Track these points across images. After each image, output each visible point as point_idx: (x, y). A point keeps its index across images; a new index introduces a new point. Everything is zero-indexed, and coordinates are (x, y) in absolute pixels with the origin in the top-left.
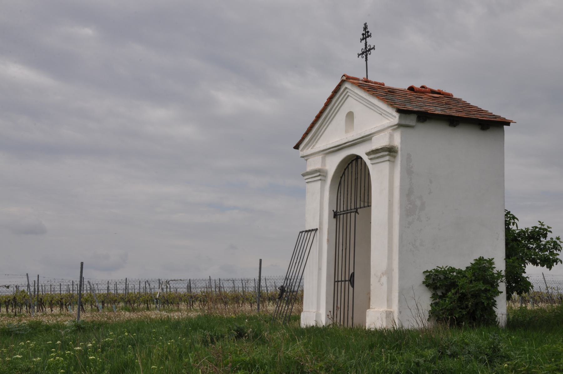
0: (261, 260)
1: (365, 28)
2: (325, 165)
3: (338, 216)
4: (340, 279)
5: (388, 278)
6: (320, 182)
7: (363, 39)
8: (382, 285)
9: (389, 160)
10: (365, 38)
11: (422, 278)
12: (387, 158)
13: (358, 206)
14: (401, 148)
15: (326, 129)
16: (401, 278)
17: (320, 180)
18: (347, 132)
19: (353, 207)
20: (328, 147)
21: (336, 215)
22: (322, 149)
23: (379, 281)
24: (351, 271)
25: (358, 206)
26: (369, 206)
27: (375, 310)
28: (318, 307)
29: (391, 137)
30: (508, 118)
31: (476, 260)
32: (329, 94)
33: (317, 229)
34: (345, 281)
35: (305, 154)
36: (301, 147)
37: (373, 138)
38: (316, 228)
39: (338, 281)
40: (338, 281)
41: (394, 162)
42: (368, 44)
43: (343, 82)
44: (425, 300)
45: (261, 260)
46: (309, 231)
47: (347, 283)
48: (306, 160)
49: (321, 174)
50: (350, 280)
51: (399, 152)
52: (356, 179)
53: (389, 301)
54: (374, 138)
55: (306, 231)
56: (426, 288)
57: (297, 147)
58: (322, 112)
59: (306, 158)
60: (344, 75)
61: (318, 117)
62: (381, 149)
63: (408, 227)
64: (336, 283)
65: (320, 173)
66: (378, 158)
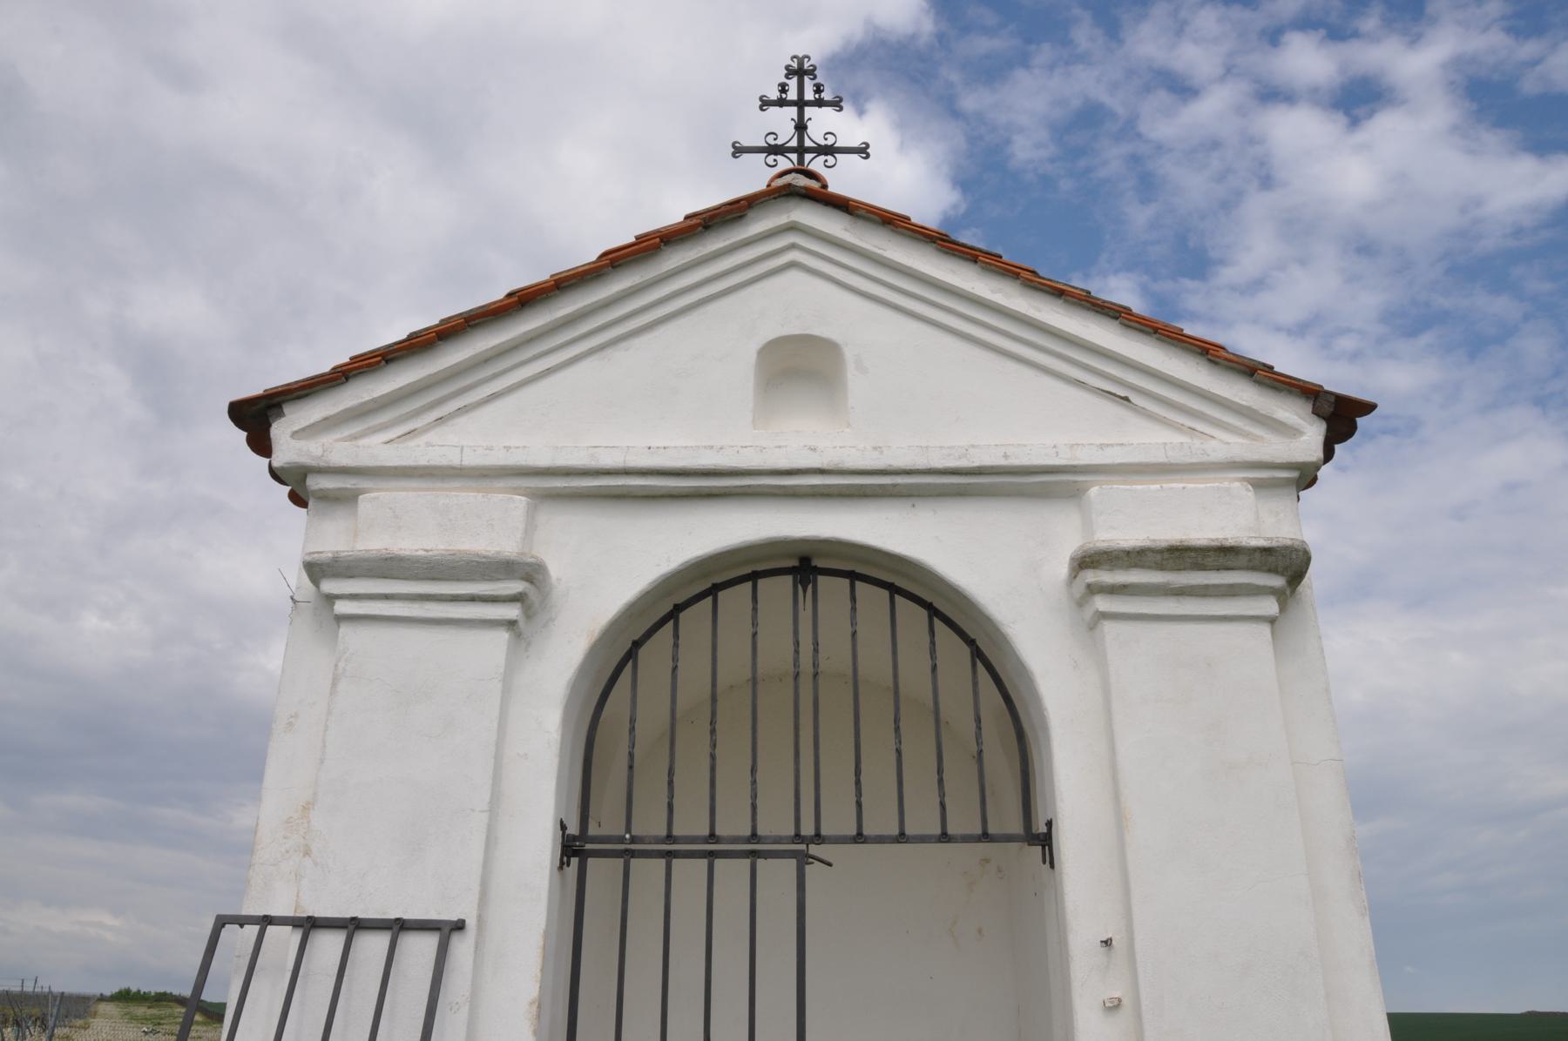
7: (781, 103)
10: (801, 104)
17: (511, 624)
21: (573, 849)
22: (543, 460)
33: (459, 926)
38: (453, 917)
49: (533, 595)
61: (523, 301)
65: (519, 589)
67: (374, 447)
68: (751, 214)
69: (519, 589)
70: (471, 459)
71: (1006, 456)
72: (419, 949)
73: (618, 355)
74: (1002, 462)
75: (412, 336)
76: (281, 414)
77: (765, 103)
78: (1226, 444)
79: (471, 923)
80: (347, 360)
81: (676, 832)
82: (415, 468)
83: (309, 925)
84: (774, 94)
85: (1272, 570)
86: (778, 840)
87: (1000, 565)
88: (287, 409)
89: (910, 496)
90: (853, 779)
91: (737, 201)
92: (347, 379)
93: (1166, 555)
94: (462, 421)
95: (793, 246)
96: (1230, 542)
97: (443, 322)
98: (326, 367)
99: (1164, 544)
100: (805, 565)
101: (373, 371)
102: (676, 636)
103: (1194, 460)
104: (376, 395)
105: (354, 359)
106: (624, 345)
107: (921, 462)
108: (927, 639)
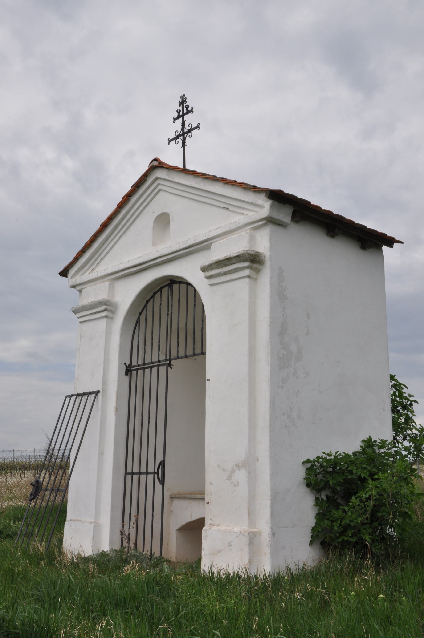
1: (183, 102)
3: (134, 373)
4: (136, 470)
5: (249, 473)
6: (105, 320)
7: (178, 118)
8: (236, 485)
9: (249, 277)
10: (183, 116)
11: (301, 473)
12: (247, 272)
13: (174, 354)
14: (270, 256)
15: (116, 243)
16: (274, 474)
17: (106, 317)
18: (154, 244)
19: (162, 357)
21: (129, 370)
22: (110, 271)
23: (229, 478)
24: (159, 459)
25: (174, 354)
27: (222, 528)
28: (97, 514)
29: (252, 239)
30: (389, 234)
31: (364, 441)
32: (128, 188)
33: (98, 392)
34: (147, 473)
35: (78, 282)
36: (72, 272)
37: (213, 245)
38: (96, 390)
39: (133, 474)
40: (133, 474)
41: (255, 279)
42: (187, 124)
43: (152, 169)
44: (305, 510)
46: (84, 394)
47: (151, 477)
48: (80, 291)
49: (108, 307)
50: (156, 473)
51: (268, 264)
52: (169, 315)
53: (251, 514)
55: (78, 395)
56: (307, 490)
57: (64, 273)
58: (111, 218)
59: (79, 288)
60: (156, 160)
61: (104, 226)
62: (238, 256)
63: (282, 387)
64: (129, 477)
65: (107, 307)
66: (225, 274)
67: (86, 276)
68: (148, 178)
69: (107, 307)
71: (195, 240)
72: (93, 396)
75: (86, 244)
76: (69, 273)
77: (175, 119)
78: (238, 219)
79: (101, 390)
80: (76, 255)
84: (176, 115)
85: (244, 261)
87: (189, 270)
89: (181, 257)
92: (78, 259)
95: (159, 184)
96: (229, 257)
97: (90, 238)
98: (72, 259)
99: (214, 262)
101: (82, 256)
102: (147, 311)
103: (236, 227)
106: (129, 229)
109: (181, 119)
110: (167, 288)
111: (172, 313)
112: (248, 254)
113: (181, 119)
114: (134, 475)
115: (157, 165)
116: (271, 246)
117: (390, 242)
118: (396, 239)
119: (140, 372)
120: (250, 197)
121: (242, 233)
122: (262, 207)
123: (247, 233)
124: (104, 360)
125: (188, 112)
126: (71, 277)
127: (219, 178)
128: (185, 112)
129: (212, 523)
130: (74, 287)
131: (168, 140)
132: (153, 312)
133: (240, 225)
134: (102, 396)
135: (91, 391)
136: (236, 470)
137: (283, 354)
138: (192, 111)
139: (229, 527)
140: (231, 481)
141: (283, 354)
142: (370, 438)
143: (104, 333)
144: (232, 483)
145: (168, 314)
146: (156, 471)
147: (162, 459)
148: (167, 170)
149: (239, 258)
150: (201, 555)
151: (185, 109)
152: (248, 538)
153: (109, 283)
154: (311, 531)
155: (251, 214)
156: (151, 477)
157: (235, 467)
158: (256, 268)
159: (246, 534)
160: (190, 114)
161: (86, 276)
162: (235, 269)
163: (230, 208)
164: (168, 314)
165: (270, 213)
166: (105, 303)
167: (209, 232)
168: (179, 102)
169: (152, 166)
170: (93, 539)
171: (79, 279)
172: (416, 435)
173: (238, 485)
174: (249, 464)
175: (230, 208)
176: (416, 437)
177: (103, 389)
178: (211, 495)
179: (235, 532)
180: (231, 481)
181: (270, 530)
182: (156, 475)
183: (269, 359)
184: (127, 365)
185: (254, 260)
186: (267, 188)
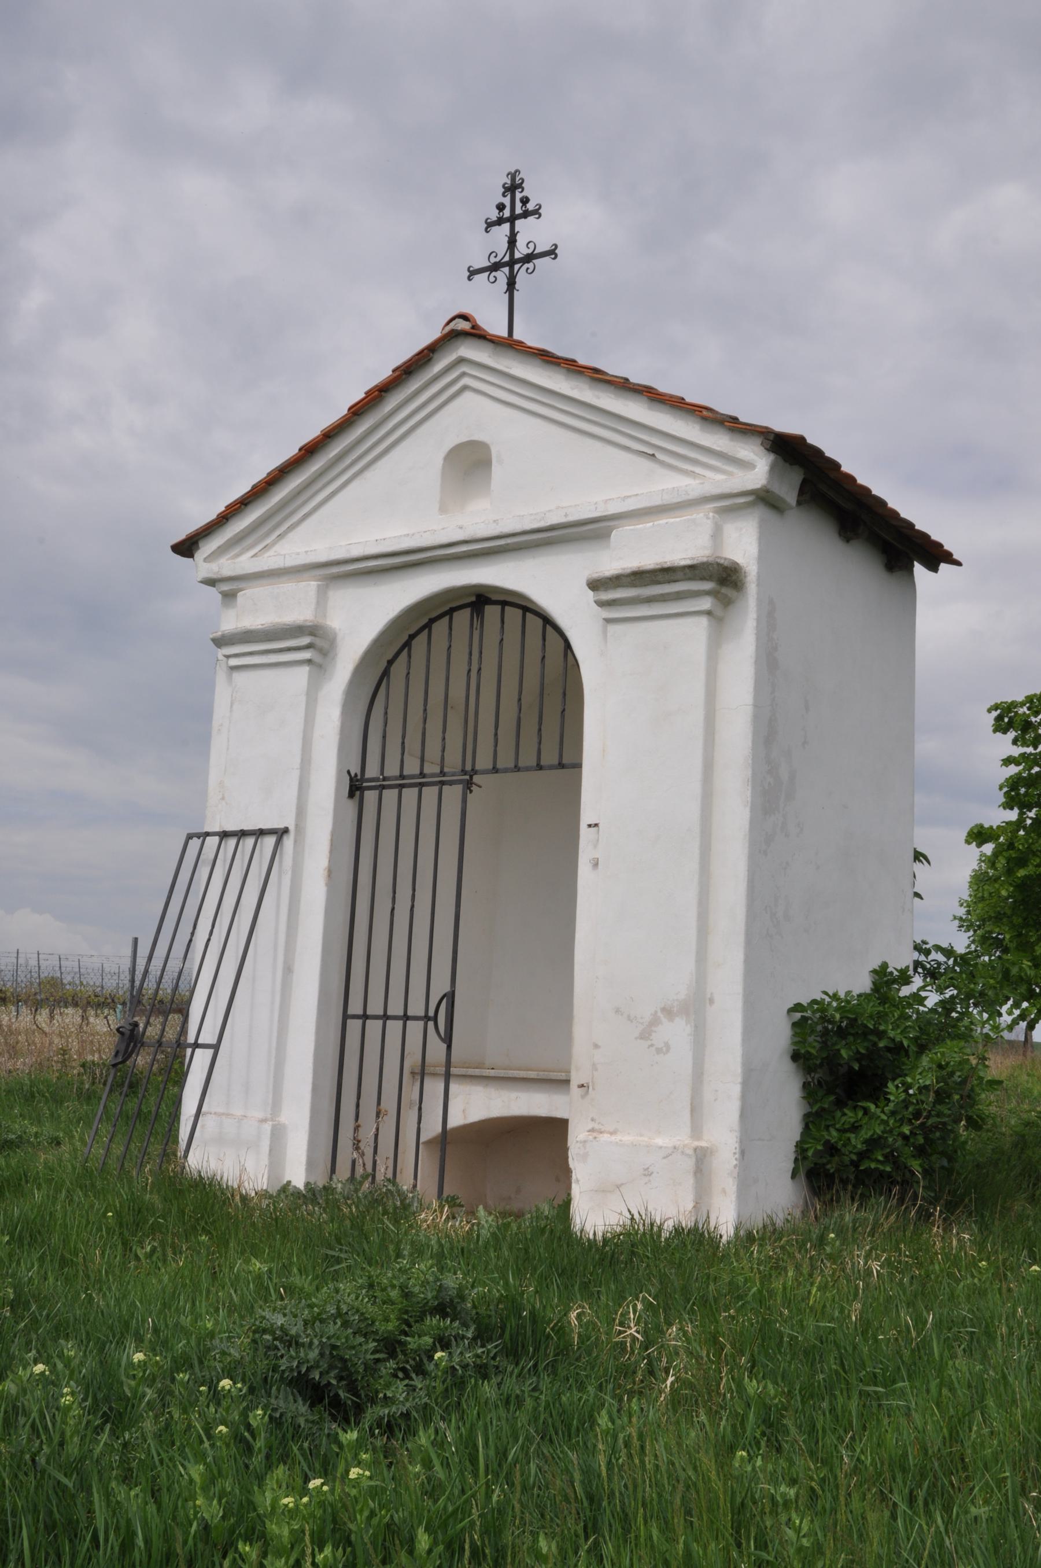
0: (136, 940)
2: (325, 616)
3: (371, 796)
5: (696, 1027)
6: (306, 669)
7: (500, 221)
9: (709, 613)
10: (512, 219)
13: (483, 761)
17: (309, 662)
18: (443, 509)
20: (356, 552)
21: (355, 787)
22: (323, 558)
23: (645, 1035)
24: (440, 986)
25: (483, 761)
26: (569, 764)
29: (717, 535)
31: (874, 971)
33: (286, 831)
35: (227, 572)
36: (207, 547)
38: (282, 826)
43: (451, 337)
45: (136, 940)
46: (242, 834)
47: (415, 1028)
49: (318, 642)
51: (752, 588)
54: (621, 534)
58: (329, 436)
59: (225, 587)
62: (692, 567)
64: (354, 1025)
65: (313, 642)
67: (244, 562)
68: (436, 356)
69: (313, 642)
70: (290, 562)
71: (566, 515)
72: (270, 841)
73: (368, 474)
74: (563, 520)
75: (254, 487)
76: (198, 548)
77: (489, 225)
79: (292, 828)
81: (405, 773)
82: (263, 572)
83: (224, 835)
84: (494, 215)
85: (703, 579)
86: (433, 775)
87: (554, 585)
88: (201, 544)
89: (521, 549)
90: (400, 741)
91: (422, 352)
92: (227, 520)
93: (633, 578)
94: (291, 535)
97: (269, 474)
98: (213, 516)
99: (629, 571)
100: (480, 599)
102: (409, 656)
104: (242, 527)
105: (228, 507)
107: (518, 527)
108: (540, 642)
109: (506, 226)
110: (468, 610)
111: (480, 669)
112: (718, 564)
113: (506, 226)
114: (388, 1022)
115: (464, 330)
116: (760, 551)
117: (935, 555)
118: (955, 557)
119: (391, 795)
120: (719, 440)
121: (694, 516)
122: (745, 465)
123: (708, 518)
124: (302, 760)
125: (526, 214)
126: (205, 560)
127: (634, 384)
128: (518, 210)
129: (597, 1126)
130: (211, 582)
131: (469, 270)
132: (428, 660)
133: (690, 497)
134: (295, 841)
135: (245, 828)
136: (664, 1020)
137: (769, 784)
138: (536, 212)
139: (641, 1136)
140: (649, 1043)
141: (769, 784)
142: (884, 966)
143: (303, 698)
144: (652, 1045)
145: (469, 671)
146: (431, 1013)
147: (447, 988)
148: (491, 345)
149: (693, 571)
150: (569, 1194)
151: (518, 204)
152: (694, 1159)
153: (319, 586)
154: (793, 1149)
155: (720, 477)
156: (415, 1028)
157: (659, 1014)
158: (726, 596)
159: (691, 1152)
160: (531, 219)
161: (244, 562)
162: (678, 593)
163: (660, 456)
164: (469, 671)
165: (768, 482)
166: (312, 630)
167: (606, 501)
168: (504, 186)
169: (452, 331)
170: (270, 1154)
171: (226, 566)
172: (939, 964)
173: (668, 1050)
174: (695, 1008)
175: (660, 456)
176: (939, 967)
177: (297, 826)
178: (596, 1070)
179: (661, 1147)
180: (649, 1043)
181: (737, 1145)
182: (431, 1024)
183: (749, 793)
184: (353, 775)
185: (725, 578)
186: (766, 428)
